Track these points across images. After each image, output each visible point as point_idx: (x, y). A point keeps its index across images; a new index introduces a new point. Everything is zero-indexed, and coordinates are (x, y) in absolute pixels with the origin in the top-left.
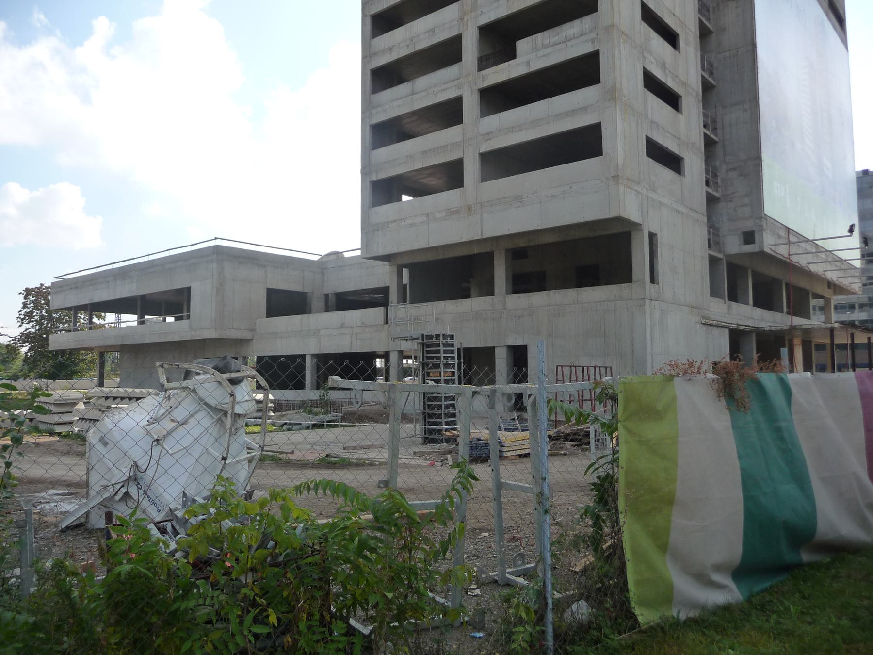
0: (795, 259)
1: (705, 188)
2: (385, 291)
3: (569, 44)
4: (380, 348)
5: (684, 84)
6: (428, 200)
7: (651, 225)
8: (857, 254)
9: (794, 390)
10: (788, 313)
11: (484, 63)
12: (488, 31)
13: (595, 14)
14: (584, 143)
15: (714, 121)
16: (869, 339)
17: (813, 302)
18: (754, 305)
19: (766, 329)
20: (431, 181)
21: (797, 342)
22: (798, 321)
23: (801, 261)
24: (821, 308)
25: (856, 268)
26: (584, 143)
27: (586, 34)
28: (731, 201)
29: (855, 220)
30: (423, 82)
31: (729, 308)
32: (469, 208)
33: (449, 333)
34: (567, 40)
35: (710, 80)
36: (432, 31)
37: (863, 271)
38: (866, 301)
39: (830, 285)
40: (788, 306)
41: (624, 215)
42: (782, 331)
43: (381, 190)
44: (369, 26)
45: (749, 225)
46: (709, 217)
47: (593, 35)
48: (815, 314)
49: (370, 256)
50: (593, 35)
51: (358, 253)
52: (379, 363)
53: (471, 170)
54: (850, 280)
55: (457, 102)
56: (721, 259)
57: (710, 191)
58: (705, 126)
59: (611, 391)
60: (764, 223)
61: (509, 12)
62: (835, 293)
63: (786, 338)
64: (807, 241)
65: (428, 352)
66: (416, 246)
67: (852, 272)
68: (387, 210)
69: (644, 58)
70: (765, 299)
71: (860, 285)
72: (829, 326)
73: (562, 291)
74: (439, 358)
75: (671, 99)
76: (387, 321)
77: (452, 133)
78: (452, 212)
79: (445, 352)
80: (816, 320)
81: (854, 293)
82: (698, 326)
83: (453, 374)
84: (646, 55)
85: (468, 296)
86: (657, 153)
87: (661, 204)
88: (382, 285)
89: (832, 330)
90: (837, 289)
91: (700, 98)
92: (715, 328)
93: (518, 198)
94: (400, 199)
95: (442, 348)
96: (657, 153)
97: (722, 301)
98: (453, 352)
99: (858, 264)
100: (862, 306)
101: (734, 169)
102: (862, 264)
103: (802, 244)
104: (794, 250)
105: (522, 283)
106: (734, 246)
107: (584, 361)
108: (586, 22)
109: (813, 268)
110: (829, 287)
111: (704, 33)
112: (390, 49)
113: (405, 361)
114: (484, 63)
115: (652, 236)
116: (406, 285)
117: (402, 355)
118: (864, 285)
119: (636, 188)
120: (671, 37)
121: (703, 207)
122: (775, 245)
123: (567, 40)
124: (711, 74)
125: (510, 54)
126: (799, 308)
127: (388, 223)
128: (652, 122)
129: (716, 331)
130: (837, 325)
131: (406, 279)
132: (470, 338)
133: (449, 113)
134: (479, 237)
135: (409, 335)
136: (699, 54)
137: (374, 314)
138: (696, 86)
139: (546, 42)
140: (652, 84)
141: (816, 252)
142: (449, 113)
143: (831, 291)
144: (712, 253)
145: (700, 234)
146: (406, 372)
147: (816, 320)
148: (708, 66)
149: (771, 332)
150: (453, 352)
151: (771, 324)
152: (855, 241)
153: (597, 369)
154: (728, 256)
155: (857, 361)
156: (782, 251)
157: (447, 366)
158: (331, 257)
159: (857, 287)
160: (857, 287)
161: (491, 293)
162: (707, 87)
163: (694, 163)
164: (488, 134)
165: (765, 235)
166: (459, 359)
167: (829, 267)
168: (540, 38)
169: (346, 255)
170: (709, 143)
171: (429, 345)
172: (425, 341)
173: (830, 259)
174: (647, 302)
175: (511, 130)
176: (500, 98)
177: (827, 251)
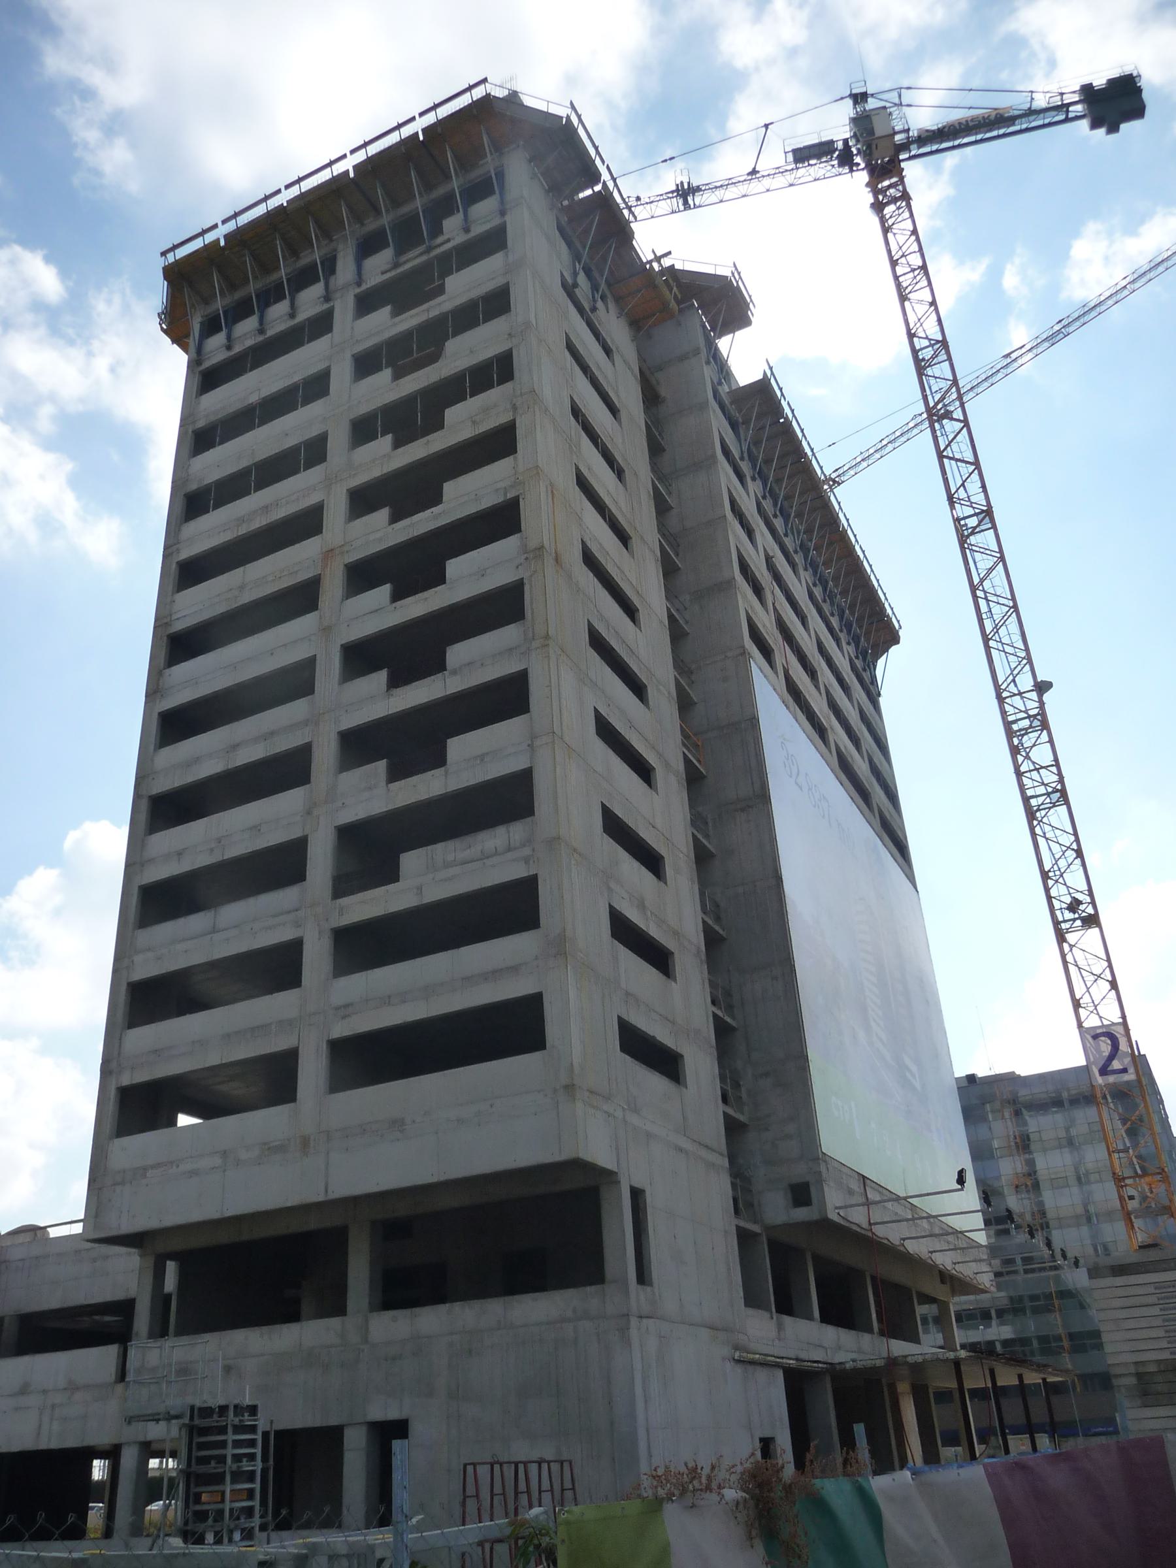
0: (880, 1231)
1: (721, 1107)
2: (125, 1308)
3: (488, 862)
4: (103, 1439)
5: (676, 934)
6: (228, 1124)
7: (633, 1173)
8: (978, 1221)
9: (889, 1513)
10: (882, 1333)
11: (343, 886)
12: (352, 837)
13: (529, 819)
14: (512, 1028)
15: (728, 994)
16: (1020, 1377)
17: (921, 1310)
18: (822, 1321)
19: (848, 1366)
20: (235, 1089)
21: (903, 1387)
22: (900, 1348)
23: (891, 1234)
24: (937, 1320)
25: (982, 1246)
26: (512, 1028)
27: (515, 849)
28: (767, 1129)
29: (967, 1164)
30: (233, 912)
31: (780, 1327)
32: (305, 1143)
33: (247, 1401)
34: (484, 856)
35: (717, 928)
36: (256, 829)
37: (993, 1250)
38: (1004, 1303)
39: (944, 1277)
40: (880, 1320)
41: (588, 1158)
42: (874, 1369)
43: (134, 1105)
44: (143, 816)
45: (799, 1172)
46: (732, 1158)
47: (527, 851)
48: (926, 1331)
49: (103, 1234)
50: (527, 851)
51: (78, 1229)
52: (98, 1470)
53: (312, 1071)
54: (974, 1267)
55: (295, 948)
56: (759, 1234)
57: (730, 1111)
58: (713, 1003)
59: (545, 1541)
60: (823, 1168)
61: (390, 807)
62: (954, 1292)
63: (884, 1381)
64: (898, 1199)
65: (201, 1446)
66: (196, 1216)
67: (973, 1254)
68: (143, 1145)
69: (610, 889)
70: (840, 1311)
71: (991, 1276)
72: (951, 1355)
73: (477, 1305)
74: (222, 1460)
75: (658, 957)
76: (122, 1376)
77: (281, 1004)
78: (272, 1149)
79: (237, 1444)
80: (927, 1346)
81: (986, 1292)
82: (729, 1365)
83: (250, 1494)
84: (613, 885)
85: (293, 1317)
86: (640, 1046)
87: (649, 1135)
88: (120, 1295)
89: (957, 1363)
90: (956, 1284)
91: (704, 957)
92: (759, 1369)
93: (397, 1124)
94: (173, 1122)
95: (231, 1437)
96: (640, 1046)
97: (766, 1315)
98: (252, 1443)
99: (981, 1238)
100: (1001, 1313)
101: (767, 1074)
102: (988, 1236)
103: (889, 1205)
104: (877, 1215)
105: (401, 1290)
106: (777, 1210)
107: (522, 1450)
108: (517, 831)
109: (912, 1247)
110: (943, 1282)
111: (702, 857)
112: (180, 854)
113: (154, 1463)
114: (343, 886)
115: (637, 1195)
116: (169, 1296)
117: (150, 1450)
118: (998, 1275)
119: (605, 1107)
120: (652, 861)
121: (722, 1143)
122: (846, 1207)
123: (484, 856)
124: (718, 919)
125: (389, 874)
126: (899, 1325)
127: (145, 1169)
128: (628, 994)
129: (761, 1375)
130: (963, 1354)
131: (170, 1283)
132: (292, 1411)
133: (277, 968)
134: (321, 1198)
135: (161, 1408)
136: (696, 887)
137: (98, 1361)
138: (698, 939)
139: (450, 857)
140: (624, 931)
141: (913, 1219)
142: (277, 968)
143: (946, 1288)
144: (742, 1224)
145: (721, 1187)
146: (153, 1488)
147: (927, 1346)
148: (711, 907)
149: (856, 1371)
150: (252, 1443)
151: (854, 1356)
152: (970, 1198)
153: (545, 1466)
154: (768, 1229)
155: (1008, 1420)
156: (858, 1217)
157: (237, 1476)
158: (21, 1239)
159: (986, 1280)
160: (986, 1280)
161: (339, 1309)
162: (713, 941)
163: (701, 1065)
164: (346, 1006)
165: (826, 1189)
166: (265, 1459)
167: (937, 1244)
168: (441, 851)
169: (54, 1233)
170: (722, 1030)
171: (204, 1431)
172: (197, 1422)
173: (937, 1231)
174: (634, 1321)
175: (387, 1001)
176: (363, 947)
177: (930, 1216)
